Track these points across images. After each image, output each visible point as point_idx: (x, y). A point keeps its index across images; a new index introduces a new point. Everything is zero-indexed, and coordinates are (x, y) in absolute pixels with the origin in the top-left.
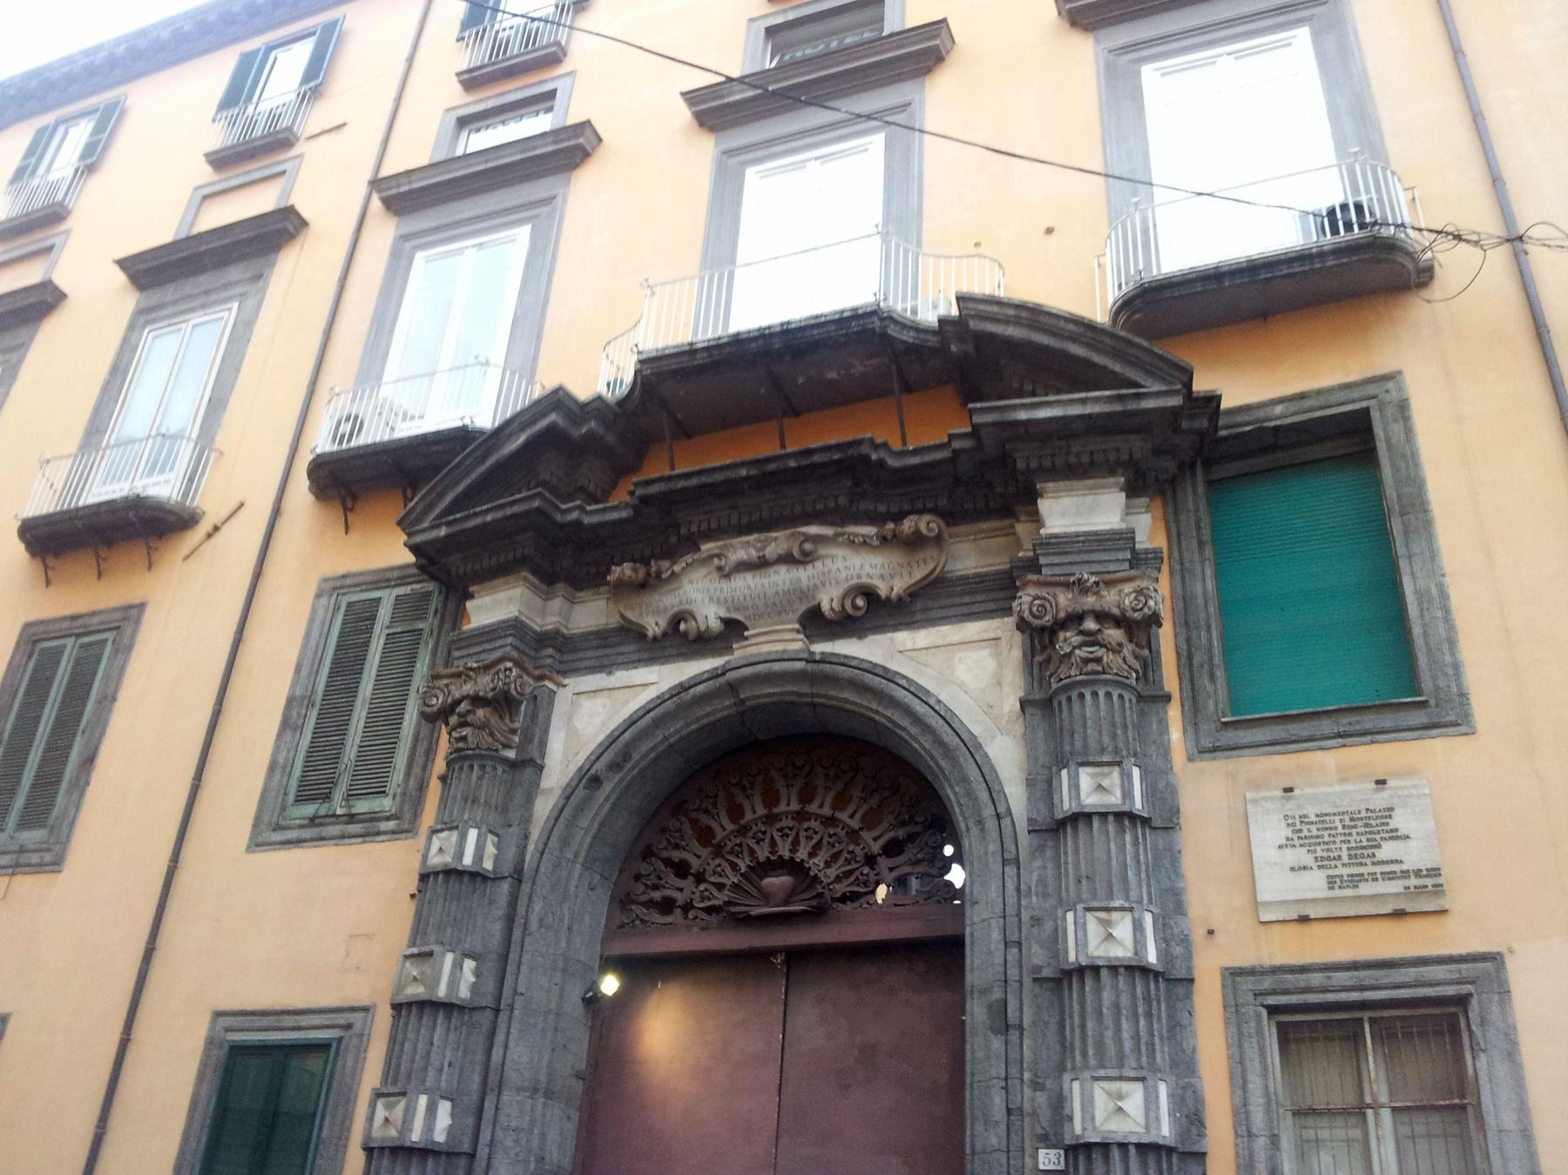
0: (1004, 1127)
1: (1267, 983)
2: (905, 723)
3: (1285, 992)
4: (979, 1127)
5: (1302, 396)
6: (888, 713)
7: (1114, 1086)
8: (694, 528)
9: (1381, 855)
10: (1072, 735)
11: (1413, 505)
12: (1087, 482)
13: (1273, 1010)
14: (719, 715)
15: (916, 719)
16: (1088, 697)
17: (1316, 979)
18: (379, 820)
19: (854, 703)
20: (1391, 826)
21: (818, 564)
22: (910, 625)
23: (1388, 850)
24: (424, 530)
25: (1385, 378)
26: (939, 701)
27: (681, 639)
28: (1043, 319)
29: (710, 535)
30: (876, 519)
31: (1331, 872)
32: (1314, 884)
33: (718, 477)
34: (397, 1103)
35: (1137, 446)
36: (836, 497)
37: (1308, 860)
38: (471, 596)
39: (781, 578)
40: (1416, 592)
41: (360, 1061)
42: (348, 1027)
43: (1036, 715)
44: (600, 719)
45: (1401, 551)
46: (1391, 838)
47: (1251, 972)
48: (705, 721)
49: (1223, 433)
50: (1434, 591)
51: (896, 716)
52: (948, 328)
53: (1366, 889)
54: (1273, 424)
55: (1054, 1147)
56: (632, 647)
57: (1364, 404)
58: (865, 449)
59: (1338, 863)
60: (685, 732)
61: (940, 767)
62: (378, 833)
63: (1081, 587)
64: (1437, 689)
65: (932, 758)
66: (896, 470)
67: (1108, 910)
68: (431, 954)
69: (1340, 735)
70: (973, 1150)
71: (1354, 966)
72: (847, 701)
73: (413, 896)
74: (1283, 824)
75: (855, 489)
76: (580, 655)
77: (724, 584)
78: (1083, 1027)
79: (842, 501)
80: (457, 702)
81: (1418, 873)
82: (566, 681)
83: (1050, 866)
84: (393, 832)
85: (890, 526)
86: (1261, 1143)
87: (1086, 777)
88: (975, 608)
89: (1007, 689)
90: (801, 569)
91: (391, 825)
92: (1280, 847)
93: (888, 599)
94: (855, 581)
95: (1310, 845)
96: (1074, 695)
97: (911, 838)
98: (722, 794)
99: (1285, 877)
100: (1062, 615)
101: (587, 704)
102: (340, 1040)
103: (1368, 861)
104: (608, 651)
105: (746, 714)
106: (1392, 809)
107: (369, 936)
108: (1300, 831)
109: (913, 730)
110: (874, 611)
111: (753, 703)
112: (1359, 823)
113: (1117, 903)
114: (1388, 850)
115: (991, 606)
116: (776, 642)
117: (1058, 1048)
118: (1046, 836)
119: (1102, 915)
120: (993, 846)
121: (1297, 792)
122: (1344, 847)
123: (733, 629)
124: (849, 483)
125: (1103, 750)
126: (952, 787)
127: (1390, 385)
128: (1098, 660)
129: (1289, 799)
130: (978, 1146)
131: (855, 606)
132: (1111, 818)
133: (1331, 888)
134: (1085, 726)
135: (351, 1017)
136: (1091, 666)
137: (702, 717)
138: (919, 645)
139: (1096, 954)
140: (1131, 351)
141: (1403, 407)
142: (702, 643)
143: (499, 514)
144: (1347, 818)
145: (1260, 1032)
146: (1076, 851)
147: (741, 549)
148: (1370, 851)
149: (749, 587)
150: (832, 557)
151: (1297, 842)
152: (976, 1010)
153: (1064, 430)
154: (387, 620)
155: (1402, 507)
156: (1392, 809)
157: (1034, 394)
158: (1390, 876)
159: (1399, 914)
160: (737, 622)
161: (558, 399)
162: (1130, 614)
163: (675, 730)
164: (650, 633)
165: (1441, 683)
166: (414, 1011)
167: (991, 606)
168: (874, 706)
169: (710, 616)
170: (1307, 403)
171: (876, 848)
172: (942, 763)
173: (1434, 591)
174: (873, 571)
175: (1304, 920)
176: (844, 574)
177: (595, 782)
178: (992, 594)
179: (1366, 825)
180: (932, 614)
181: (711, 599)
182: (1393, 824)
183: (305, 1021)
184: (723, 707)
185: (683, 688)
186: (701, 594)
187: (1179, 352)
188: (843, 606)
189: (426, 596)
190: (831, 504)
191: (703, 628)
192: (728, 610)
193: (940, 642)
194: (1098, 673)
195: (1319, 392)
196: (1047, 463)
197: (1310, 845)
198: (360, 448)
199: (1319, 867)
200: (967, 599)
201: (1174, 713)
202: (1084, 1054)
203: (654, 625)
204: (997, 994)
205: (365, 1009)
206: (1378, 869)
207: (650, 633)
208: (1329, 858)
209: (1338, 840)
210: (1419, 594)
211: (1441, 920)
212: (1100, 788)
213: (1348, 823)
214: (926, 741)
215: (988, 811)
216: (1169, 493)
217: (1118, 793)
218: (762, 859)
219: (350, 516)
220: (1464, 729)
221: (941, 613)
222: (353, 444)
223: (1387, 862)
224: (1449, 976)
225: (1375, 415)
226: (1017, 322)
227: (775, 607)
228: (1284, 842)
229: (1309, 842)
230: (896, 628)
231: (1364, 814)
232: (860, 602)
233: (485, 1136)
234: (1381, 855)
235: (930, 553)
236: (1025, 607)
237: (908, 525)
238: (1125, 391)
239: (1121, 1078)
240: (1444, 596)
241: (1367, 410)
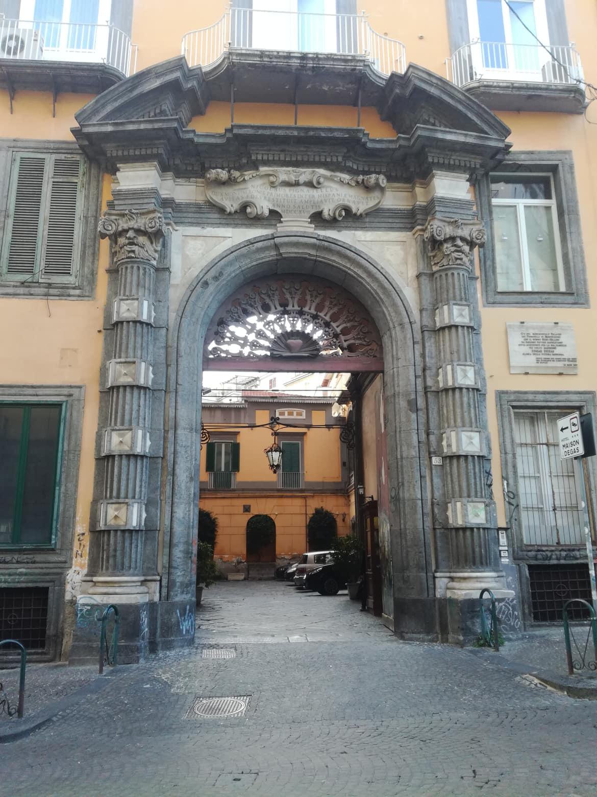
0: (417, 448)
1: (512, 398)
2: (364, 276)
3: (519, 401)
4: (404, 448)
5: (532, 153)
6: (356, 270)
7: (469, 434)
8: (260, 157)
9: (556, 351)
10: (448, 291)
11: (573, 211)
12: (452, 174)
13: (514, 407)
14: (267, 259)
15: (370, 274)
16: (456, 275)
17: (531, 397)
18: (68, 288)
19: (339, 264)
20: (560, 341)
21: (324, 190)
22: (363, 228)
23: (559, 350)
24: (94, 125)
25: (565, 152)
26: (382, 268)
27: (244, 215)
28: (448, 88)
29: (266, 163)
30: (350, 171)
31: (538, 357)
32: (531, 361)
33: (267, 132)
34: (127, 433)
35: (476, 161)
36: (337, 156)
37: (530, 351)
38: (118, 170)
39: (305, 193)
40: (572, 248)
41: (81, 413)
42: (71, 395)
43: (425, 280)
44: (200, 252)
45: (568, 230)
46: (560, 346)
47: (506, 392)
48: (261, 261)
49: (505, 162)
50: (579, 249)
51: (360, 272)
52: (396, 79)
53: (550, 364)
54: (520, 163)
55: (439, 456)
56: (216, 216)
57: (556, 162)
58: (361, 135)
59: (541, 353)
60: (250, 265)
61: (380, 298)
62: (69, 296)
63: (454, 223)
64: (577, 289)
65: (377, 293)
66: (369, 149)
67: (465, 365)
68: (134, 363)
69: (542, 303)
70: (402, 456)
71: (544, 393)
72: (334, 261)
73: (99, 331)
74: (521, 336)
75: (345, 153)
76: (185, 215)
77: (273, 190)
78: (454, 411)
79: (340, 159)
80: (127, 231)
81: (569, 360)
82: (177, 228)
83: (433, 345)
84: (79, 296)
85: (361, 177)
86: (510, 456)
87: (456, 309)
88: (394, 225)
89: (409, 266)
90: (315, 190)
91: (77, 292)
92: (519, 345)
93: (355, 214)
94: (341, 202)
95: (531, 345)
96: (449, 273)
97: (354, 327)
98: (257, 299)
99: (522, 357)
100: (448, 236)
101: (192, 243)
102: (67, 401)
103: (551, 353)
104: (202, 215)
105: (281, 260)
106: (560, 334)
107: (75, 351)
108: (527, 339)
109: (368, 280)
110: (348, 217)
111: (286, 255)
112: (549, 339)
113: (469, 363)
114: (559, 350)
115: (401, 225)
116: (296, 225)
117: (438, 418)
118: (432, 332)
119: (463, 367)
120: (409, 336)
121: (525, 324)
122: (543, 347)
123: (275, 215)
124: (345, 151)
125: (461, 299)
126: (386, 308)
127: (567, 156)
128: (461, 259)
129: (523, 326)
130: (404, 456)
131: (340, 215)
132: (465, 328)
133: (538, 363)
134: (454, 288)
135: (73, 391)
136: (459, 262)
137: (259, 259)
138: (367, 239)
139: (461, 383)
140: (486, 116)
141: (571, 167)
142: (257, 220)
143: (149, 126)
144: (544, 336)
145: (510, 415)
146: (450, 340)
147: (284, 173)
148: (552, 350)
149: (287, 195)
150: (331, 187)
151: (526, 344)
152: (401, 403)
153: (453, 147)
154: (52, 174)
155: (569, 211)
156: (560, 334)
157: (434, 125)
158: (559, 360)
159: (561, 374)
160: (277, 212)
161: (179, 64)
162: (475, 240)
163: (246, 263)
164: (228, 211)
165: (579, 287)
166: (444, 393)
167: (401, 225)
168: (348, 265)
169: (263, 206)
170: (533, 156)
171: (338, 330)
172: (382, 297)
173: (579, 249)
174: (350, 199)
175: (527, 374)
176: (336, 198)
177: (206, 284)
178: (411, 219)
179: (551, 340)
180: (373, 225)
181: (265, 198)
182: (522, 340)
183: (40, 391)
184: (270, 255)
185: (251, 242)
186: (258, 191)
187: (507, 121)
188: (334, 214)
189: (76, 163)
190: (335, 160)
191: (259, 213)
192: (274, 205)
193: (378, 240)
194: (460, 265)
195: (539, 152)
196: (441, 161)
197: (531, 345)
198: (22, 61)
199: (534, 354)
200: (390, 220)
201: (478, 285)
202: (455, 421)
203: (231, 206)
204: (413, 397)
205: (80, 387)
206: (555, 357)
207: (228, 211)
208: (537, 351)
209: (541, 344)
210: (573, 249)
211: (574, 378)
212: (461, 315)
213: (544, 338)
214: (375, 286)
215: (407, 320)
216: (477, 186)
217: (468, 318)
218: (306, 332)
219: (56, 104)
220: (586, 306)
221: (378, 225)
222: (18, 57)
223: (557, 354)
224: (577, 399)
225: (560, 168)
226: (437, 86)
227: (299, 209)
228: (521, 343)
229: (530, 344)
230: (356, 228)
231: (550, 335)
232: (344, 213)
233: (171, 449)
234: (556, 351)
235: (377, 194)
236: (435, 230)
237: (373, 178)
238: (482, 135)
239: (472, 431)
240: (582, 251)
241: (557, 165)
